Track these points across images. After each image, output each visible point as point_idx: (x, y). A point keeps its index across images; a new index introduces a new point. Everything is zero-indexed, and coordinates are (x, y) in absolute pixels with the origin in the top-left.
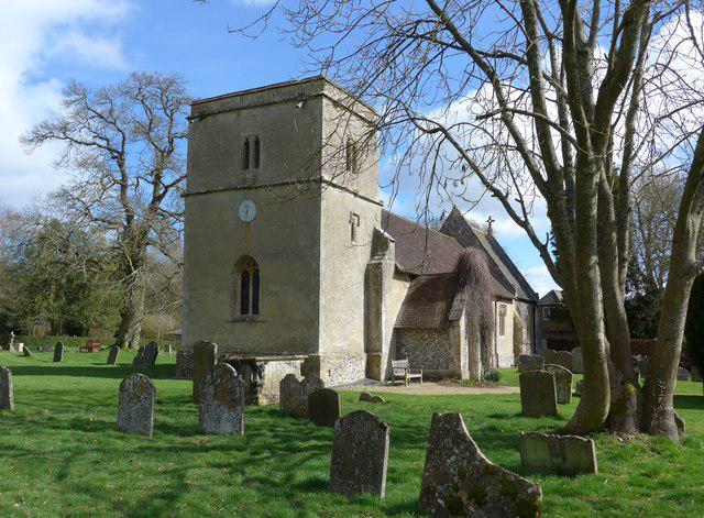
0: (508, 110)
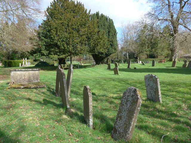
0: (102, 85)
